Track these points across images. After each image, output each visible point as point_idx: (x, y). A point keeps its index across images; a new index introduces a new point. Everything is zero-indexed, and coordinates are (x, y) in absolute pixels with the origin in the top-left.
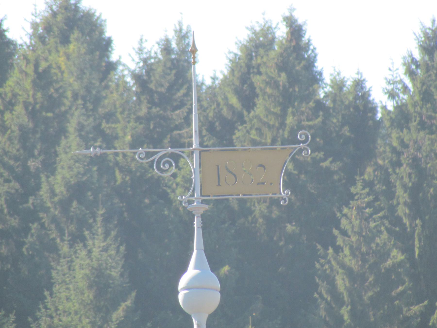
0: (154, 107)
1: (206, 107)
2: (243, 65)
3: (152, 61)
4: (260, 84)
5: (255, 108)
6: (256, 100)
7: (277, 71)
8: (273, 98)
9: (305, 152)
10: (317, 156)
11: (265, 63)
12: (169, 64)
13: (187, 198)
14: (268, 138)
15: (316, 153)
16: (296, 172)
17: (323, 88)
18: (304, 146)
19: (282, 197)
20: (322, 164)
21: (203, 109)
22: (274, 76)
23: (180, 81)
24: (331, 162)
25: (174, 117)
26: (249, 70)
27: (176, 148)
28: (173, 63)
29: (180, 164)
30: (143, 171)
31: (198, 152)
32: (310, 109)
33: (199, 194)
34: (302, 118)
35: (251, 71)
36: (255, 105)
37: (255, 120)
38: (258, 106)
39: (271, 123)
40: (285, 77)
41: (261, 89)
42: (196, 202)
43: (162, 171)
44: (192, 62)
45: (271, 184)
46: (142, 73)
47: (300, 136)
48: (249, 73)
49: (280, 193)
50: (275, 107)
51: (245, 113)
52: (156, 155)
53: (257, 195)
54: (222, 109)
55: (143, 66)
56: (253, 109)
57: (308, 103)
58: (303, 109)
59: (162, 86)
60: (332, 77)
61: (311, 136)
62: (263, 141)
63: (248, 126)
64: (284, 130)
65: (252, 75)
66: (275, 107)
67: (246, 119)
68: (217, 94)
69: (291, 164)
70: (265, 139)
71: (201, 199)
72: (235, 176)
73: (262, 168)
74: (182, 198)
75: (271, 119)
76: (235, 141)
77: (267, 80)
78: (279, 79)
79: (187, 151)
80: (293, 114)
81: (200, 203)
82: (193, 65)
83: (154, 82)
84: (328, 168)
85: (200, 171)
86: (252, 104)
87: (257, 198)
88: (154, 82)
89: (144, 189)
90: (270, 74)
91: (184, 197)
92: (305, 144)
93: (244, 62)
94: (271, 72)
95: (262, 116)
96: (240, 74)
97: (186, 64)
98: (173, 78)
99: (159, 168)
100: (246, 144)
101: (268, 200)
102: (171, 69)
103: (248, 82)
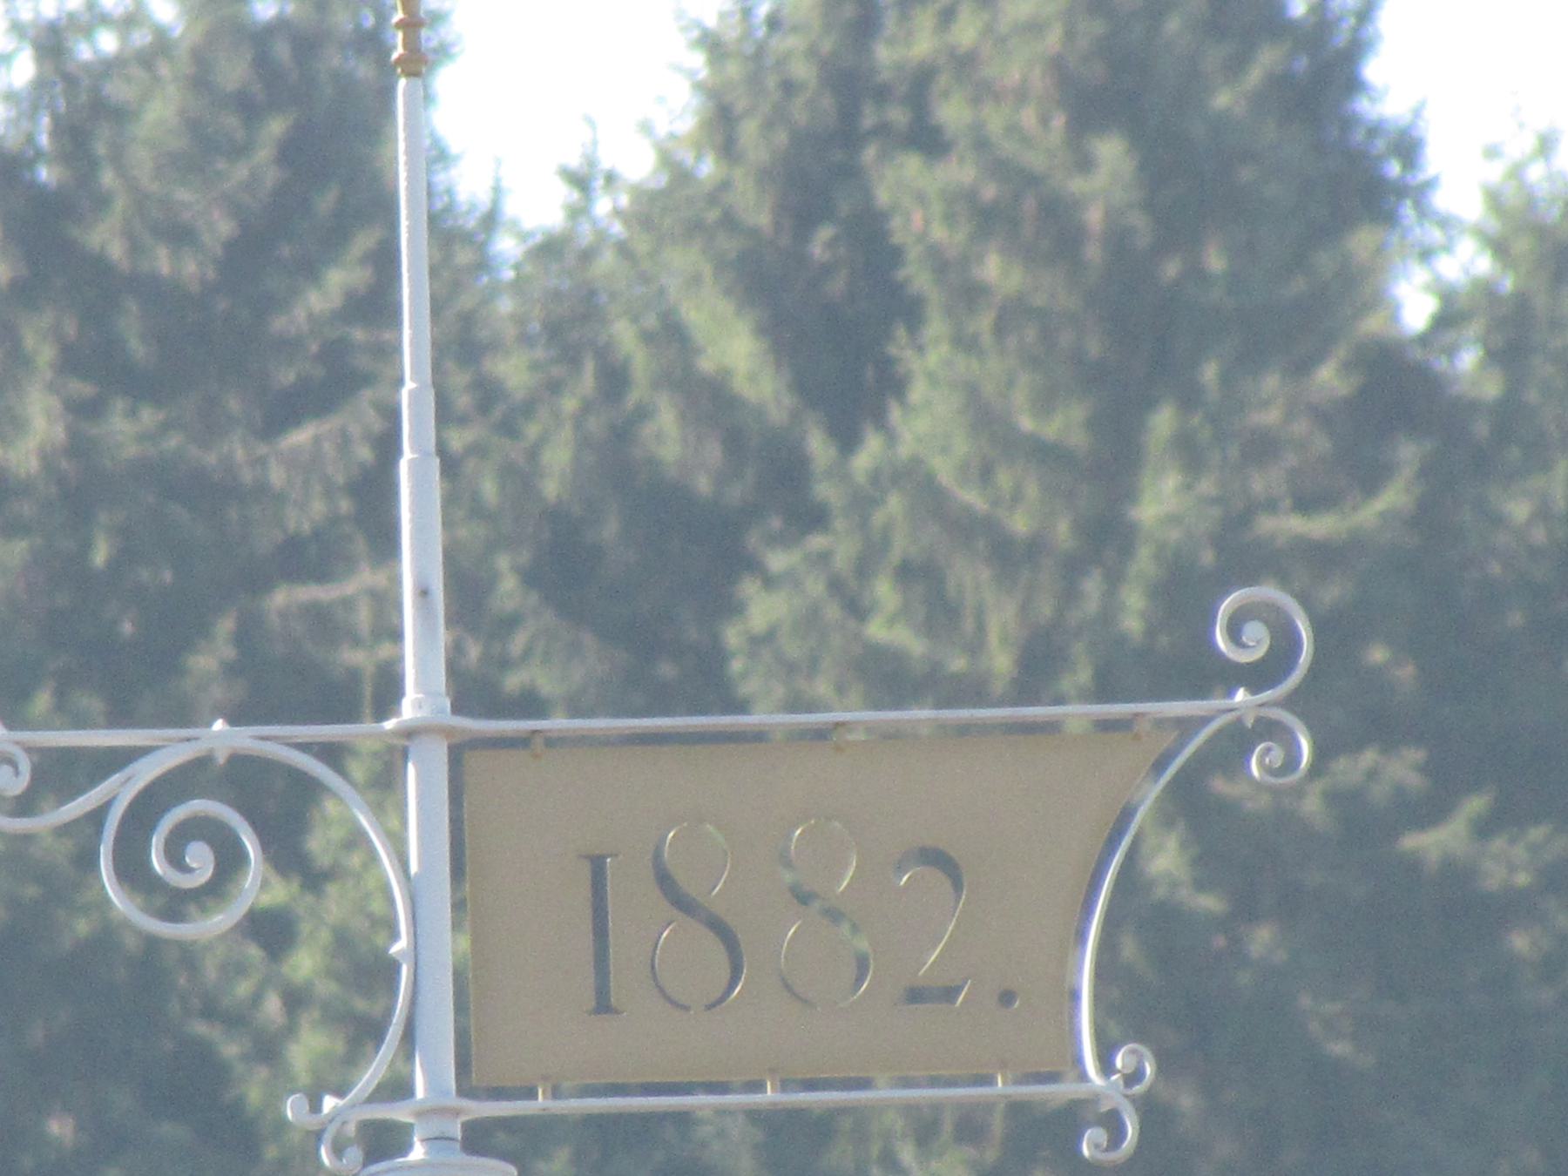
0: (119, 404)
1: (519, 395)
2: (803, 70)
3: (108, 42)
4: (927, 222)
5: (895, 414)
6: (899, 347)
7: (1059, 122)
8: (1031, 334)
9: (1268, 750)
10: (1373, 774)
11: (965, 63)
12: (234, 72)
13: (353, 1106)
14: (993, 638)
15: (1369, 757)
16: (1210, 903)
17: (1426, 255)
18: (1262, 705)
19: (1094, 1099)
20: (1412, 841)
21: (497, 413)
22: (1035, 161)
23: (326, 202)
24: (1484, 829)
25: (277, 476)
26: (849, 112)
27: (267, 721)
28: (262, 61)
29: (319, 844)
30: (32, 891)
31: (439, 754)
32: (1323, 417)
33: (452, 1084)
34: (1259, 484)
35: (869, 119)
36: (893, 384)
37: (895, 504)
38: (918, 392)
39: (1020, 524)
40: (1127, 166)
41: (940, 263)
42: (424, 1140)
43: (175, 905)
44: (395, 56)
45: (1007, 998)
46: (30, 139)
47: (1234, 633)
48: (847, 135)
49: (1083, 1077)
50: (1045, 403)
51: (819, 447)
52: (116, 778)
53: (907, 1083)
54: (643, 413)
55: (40, 84)
56: (880, 420)
57: (1302, 368)
58: (1271, 417)
59: (180, 235)
60: (1495, 172)
61: (1319, 627)
62: (958, 663)
63: (842, 546)
64: (1114, 579)
65: (870, 153)
66: (1045, 403)
67: (826, 491)
68: (603, 298)
69: (1172, 842)
70: (976, 647)
71: (464, 1118)
72: (719, 928)
73: (938, 880)
74: (316, 1107)
75: (1017, 497)
76: (736, 666)
77: (989, 192)
78: (1078, 185)
79: (368, 746)
80: (1189, 453)
81: (458, 1146)
82: (402, 83)
83: (120, 204)
84: (1457, 874)
85: (458, 906)
86: (870, 373)
87: (909, 1109)
88: (120, 204)
89: (36, 1035)
90: (1008, 148)
91: (329, 1103)
92: (1267, 695)
93: (812, 52)
94: (1012, 129)
95: (944, 470)
96: (782, 137)
97: (363, 70)
98: (272, 176)
99: (133, 871)
100: (822, 687)
101: (997, 1125)
102: (249, 108)
103: (844, 208)
